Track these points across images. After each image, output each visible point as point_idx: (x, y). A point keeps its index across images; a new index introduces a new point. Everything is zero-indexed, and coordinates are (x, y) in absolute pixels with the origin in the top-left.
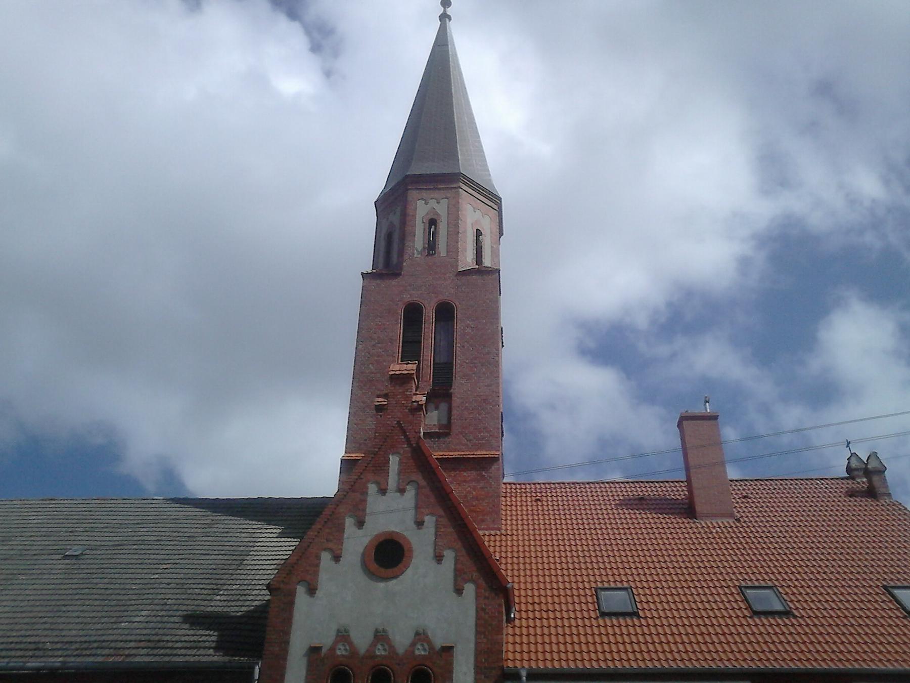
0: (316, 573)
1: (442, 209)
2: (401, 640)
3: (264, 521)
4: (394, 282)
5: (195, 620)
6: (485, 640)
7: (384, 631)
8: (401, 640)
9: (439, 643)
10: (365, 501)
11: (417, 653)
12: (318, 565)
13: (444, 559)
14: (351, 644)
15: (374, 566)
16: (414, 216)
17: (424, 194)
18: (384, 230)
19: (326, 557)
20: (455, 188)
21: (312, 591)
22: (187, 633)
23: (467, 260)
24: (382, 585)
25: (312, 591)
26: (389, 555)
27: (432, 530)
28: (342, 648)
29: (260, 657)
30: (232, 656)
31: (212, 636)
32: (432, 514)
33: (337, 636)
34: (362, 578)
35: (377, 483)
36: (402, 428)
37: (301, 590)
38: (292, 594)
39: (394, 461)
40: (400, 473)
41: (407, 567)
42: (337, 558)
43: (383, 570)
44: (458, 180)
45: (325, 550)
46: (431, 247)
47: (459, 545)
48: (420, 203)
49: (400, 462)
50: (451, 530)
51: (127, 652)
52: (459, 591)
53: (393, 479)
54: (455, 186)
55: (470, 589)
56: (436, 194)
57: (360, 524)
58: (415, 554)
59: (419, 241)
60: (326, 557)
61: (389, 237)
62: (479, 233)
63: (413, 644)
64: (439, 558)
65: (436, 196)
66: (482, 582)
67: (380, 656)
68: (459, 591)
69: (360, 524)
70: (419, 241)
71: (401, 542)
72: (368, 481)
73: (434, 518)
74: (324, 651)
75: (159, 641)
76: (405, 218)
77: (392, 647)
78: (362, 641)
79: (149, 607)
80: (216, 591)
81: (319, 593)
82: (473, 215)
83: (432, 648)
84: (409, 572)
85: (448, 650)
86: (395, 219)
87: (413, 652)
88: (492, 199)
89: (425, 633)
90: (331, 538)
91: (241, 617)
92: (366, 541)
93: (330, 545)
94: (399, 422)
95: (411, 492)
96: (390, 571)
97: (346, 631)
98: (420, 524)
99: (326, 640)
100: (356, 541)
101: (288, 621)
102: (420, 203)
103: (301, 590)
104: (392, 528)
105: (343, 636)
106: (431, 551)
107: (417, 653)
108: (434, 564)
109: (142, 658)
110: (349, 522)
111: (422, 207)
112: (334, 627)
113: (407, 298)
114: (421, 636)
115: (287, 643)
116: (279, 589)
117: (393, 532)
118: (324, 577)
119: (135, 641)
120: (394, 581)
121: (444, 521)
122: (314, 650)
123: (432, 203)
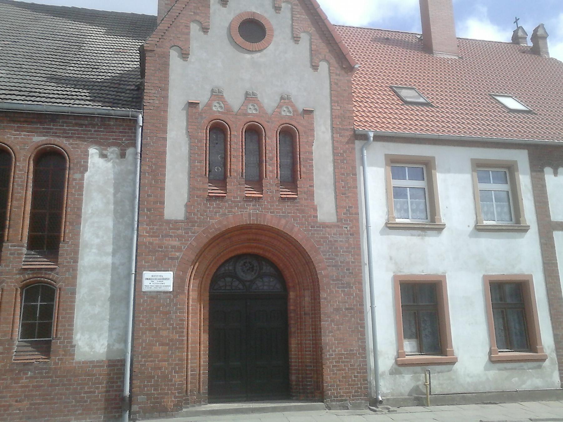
0: (187, 41)
9: (301, 107)
11: (283, 113)
12: (188, 34)
13: (301, 40)
14: (224, 102)
15: (240, 40)
19: (194, 28)
21: (185, 55)
22: (51, 87)
24: (248, 56)
25: (185, 55)
27: (289, 15)
31: (85, 93)
34: (230, 50)
37: (174, 55)
38: (166, 56)
42: (205, 30)
45: (195, 21)
47: (312, 30)
52: (315, 67)
55: (324, 66)
58: (276, 33)
60: (194, 28)
63: (279, 106)
64: (296, 39)
66: (333, 61)
67: (252, 114)
68: (315, 67)
73: (290, 6)
74: (201, 106)
77: (261, 107)
80: (67, 63)
81: (192, 58)
83: (295, 111)
84: (271, 47)
85: (308, 112)
87: (280, 113)
89: (288, 98)
92: (231, 17)
93: (198, 18)
96: (256, 46)
98: (277, 9)
103: (174, 55)
105: (217, 94)
106: (288, 31)
107: (283, 113)
108: (292, 43)
112: (209, 88)
114: (285, 99)
115: (166, 97)
117: (254, 13)
118: (194, 45)
121: (299, 8)
122: (192, 105)
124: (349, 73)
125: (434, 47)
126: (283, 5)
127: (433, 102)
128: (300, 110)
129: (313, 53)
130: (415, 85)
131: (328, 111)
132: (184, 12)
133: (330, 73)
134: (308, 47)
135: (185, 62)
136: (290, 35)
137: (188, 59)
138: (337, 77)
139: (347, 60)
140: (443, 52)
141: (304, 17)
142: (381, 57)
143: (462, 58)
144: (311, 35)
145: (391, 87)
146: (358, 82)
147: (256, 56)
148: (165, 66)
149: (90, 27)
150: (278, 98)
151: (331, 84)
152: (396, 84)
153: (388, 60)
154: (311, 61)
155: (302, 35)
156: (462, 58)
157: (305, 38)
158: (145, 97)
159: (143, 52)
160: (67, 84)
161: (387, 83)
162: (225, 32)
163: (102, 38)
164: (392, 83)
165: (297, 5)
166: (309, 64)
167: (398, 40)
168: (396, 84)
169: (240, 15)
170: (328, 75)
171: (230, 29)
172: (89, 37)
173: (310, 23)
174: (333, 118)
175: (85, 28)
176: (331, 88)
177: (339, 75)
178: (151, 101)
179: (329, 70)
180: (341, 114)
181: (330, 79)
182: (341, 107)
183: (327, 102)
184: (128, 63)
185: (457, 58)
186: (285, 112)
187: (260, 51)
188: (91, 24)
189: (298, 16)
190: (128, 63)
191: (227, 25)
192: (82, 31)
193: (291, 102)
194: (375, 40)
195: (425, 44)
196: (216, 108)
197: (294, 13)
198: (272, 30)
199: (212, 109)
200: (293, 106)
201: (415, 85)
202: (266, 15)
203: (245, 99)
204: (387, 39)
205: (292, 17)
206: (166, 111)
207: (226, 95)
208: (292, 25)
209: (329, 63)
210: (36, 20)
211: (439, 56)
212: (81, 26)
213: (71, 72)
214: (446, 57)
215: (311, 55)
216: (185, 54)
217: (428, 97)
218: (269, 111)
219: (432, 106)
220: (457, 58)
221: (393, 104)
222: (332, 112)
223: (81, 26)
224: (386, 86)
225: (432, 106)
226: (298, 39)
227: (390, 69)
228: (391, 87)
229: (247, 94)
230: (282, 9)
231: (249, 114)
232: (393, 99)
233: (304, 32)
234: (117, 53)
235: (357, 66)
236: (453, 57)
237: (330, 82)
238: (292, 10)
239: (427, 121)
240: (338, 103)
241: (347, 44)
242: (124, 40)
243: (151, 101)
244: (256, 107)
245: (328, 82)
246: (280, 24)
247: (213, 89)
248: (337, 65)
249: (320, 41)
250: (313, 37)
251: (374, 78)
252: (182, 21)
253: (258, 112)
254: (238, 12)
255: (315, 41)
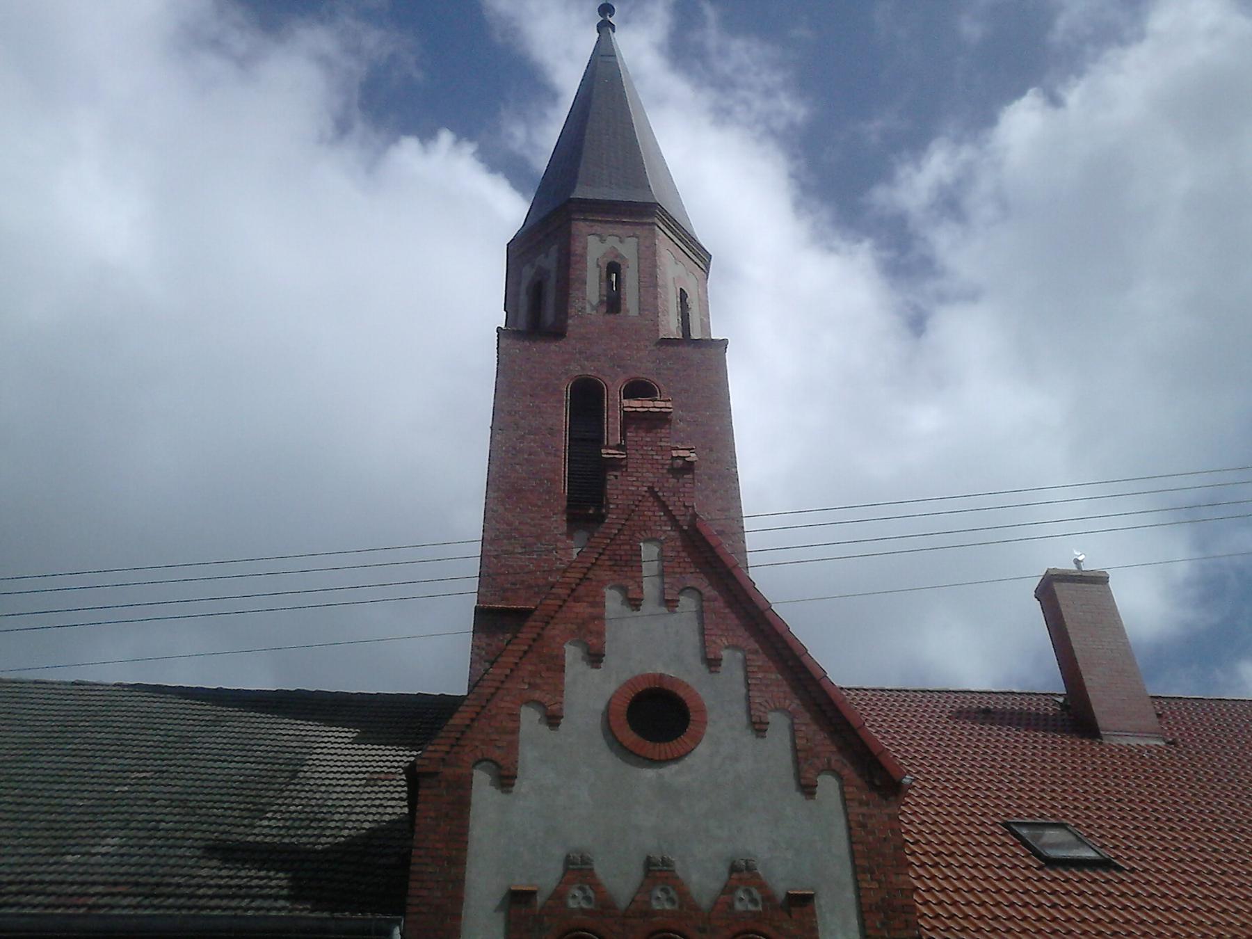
0: (513, 747)
1: (628, 250)
2: (703, 879)
3: (320, 721)
4: (553, 347)
5: (228, 852)
6: (875, 885)
7: (664, 862)
8: (703, 879)
9: (781, 888)
10: (600, 618)
11: (739, 906)
12: (515, 731)
13: (770, 728)
14: (596, 886)
15: (629, 736)
16: (583, 256)
17: (598, 228)
18: (528, 272)
19: (529, 718)
20: (645, 224)
21: (505, 780)
22: (211, 872)
23: (671, 326)
24: (650, 773)
25: (505, 780)
26: (656, 718)
27: (739, 674)
28: (577, 893)
29: (403, 913)
30: (333, 911)
31: (280, 880)
32: (735, 647)
33: (566, 870)
34: (607, 760)
35: (623, 589)
36: (657, 498)
37: (481, 780)
38: (464, 785)
39: (649, 552)
40: (662, 574)
41: (697, 740)
42: (553, 720)
43: (649, 744)
44: (653, 214)
45: (528, 702)
46: (613, 303)
47: (794, 704)
48: (592, 240)
49: (662, 558)
50: (775, 676)
51: (91, 901)
52: (808, 790)
53: (650, 587)
54: (645, 220)
55: (828, 786)
56: (619, 230)
57: (595, 658)
58: (711, 716)
59: (592, 289)
60: (529, 718)
61: (537, 292)
62: (683, 295)
63: (729, 889)
64: (759, 728)
65: (616, 232)
66: (848, 771)
67: (662, 912)
68: (808, 790)
69: (595, 658)
70: (592, 289)
71: (681, 694)
72: (603, 583)
73: (739, 655)
74: (540, 900)
75: (158, 885)
76: (567, 261)
77: (684, 894)
78: (620, 879)
79: (121, 833)
80: (261, 812)
81: (522, 785)
82: (672, 268)
83: (768, 898)
84: (702, 749)
85: (801, 902)
86: (548, 261)
87: (731, 906)
88: (700, 257)
89: (750, 868)
90: (538, 681)
91: (322, 851)
92: (611, 688)
93: (537, 695)
94: (651, 489)
95: (687, 604)
96: (665, 748)
97: (586, 861)
98: (713, 663)
99: (545, 878)
100: (589, 690)
101: (459, 837)
102: (592, 240)
103: (481, 780)
104: (660, 669)
105: (578, 869)
106: (739, 710)
107: (739, 906)
108: (748, 738)
109: (125, 909)
110: (572, 653)
111: (595, 246)
112: (559, 853)
113: (576, 370)
114: (742, 872)
115: (459, 882)
116: (436, 774)
117: (661, 676)
119: (104, 884)
120: (674, 767)
121: (760, 660)
122: (517, 899)
123: (612, 241)
124: (892, 798)
125: (1101, 723)
126: (725, 654)
127: (1117, 857)
128: (781, 896)
129: (800, 757)
130: (1065, 816)
131: (850, 894)
132: (507, 685)
133: (845, 801)
134: (788, 744)
135: (505, 796)
136: (744, 719)
137: (514, 789)
138: (864, 810)
139: (882, 768)
140: (1125, 729)
141: (773, 676)
142: (975, 753)
143: (1174, 743)
144: (792, 715)
145: (1006, 825)
146: (924, 818)
147: (669, 771)
148: (461, 805)
149: (327, 729)
150: (723, 870)
151: (849, 828)
152: (1019, 815)
153: (1014, 760)
154: (798, 775)
155: (772, 717)
156: (1174, 743)
157: (778, 724)
158: (412, 884)
159: (414, 776)
160: (246, 862)
161: (996, 815)
162: (597, 721)
163: (346, 752)
164: (1007, 815)
165: (756, 652)
166: (792, 782)
167: (1012, 712)
168: (1019, 815)
169: (630, 683)
170: (840, 807)
171: (607, 715)
172: (319, 751)
173: (788, 689)
174: (863, 913)
175: (312, 730)
176: (850, 836)
177: (868, 804)
178: (425, 893)
179: (843, 793)
180: (883, 899)
181: (847, 815)
182: (879, 882)
183: (842, 871)
184: (393, 803)
185: (1162, 744)
186: (742, 904)
187: (677, 759)
188: (330, 722)
189: (760, 676)
190: (393, 803)
191: (601, 706)
192: (306, 739)
193: (758, 876)
194: (961, 715)
195: (1073, 716)
196: (576, 900)
197: (750, 669)
198: (702, 710)
199: (565, 905)
200: (762, 886)
201: (1065, 816)
202: (687, 679)
203: (646, 876)
204: (987, 711)
205: (747, 678)
206: (458, 917)
207: (601, 870)
208: (748, 698)
209: (839, 777)
210: (216, 722)
211: (1116, 741)
212: (308, 728)
213: (266, 830)
214: (1134, 742)
215: (797, 761)
216: (508, 777)
217: (1104, 846)
218: (705, 902)
219: (1120, 869)
220: (1162, 744)
221: (1015, 867)
222: (859, 897)
223: (308, 728)
224: (994, 824)
225: (1120, 869)
226: (764, 727)
227: (1000, 782)
228: (1006, 825)
229: (649, 863)
230: (724, 664)
231: (655, 913)
232: (1016, 855)
233: (776, 710)
234: (371, 782)
235: (907, 780)
236: (1152, 742)
237: (848, 821)
238: (746, 664)
239: (1054, 906)
240: (872, 873)
241: (878, 732)
242: (393, 752)
243: (425, 893)
244: (673, 894)
245: (843, 821)
246: (721, 696)
247: (568, 856)
248: (859, 781)
249: (815, 727)
250: (796, 721)
251: (963, 805)
252: (503, 705)
253: (676, 907)
254: (626, 676)
255: (803, 728)
